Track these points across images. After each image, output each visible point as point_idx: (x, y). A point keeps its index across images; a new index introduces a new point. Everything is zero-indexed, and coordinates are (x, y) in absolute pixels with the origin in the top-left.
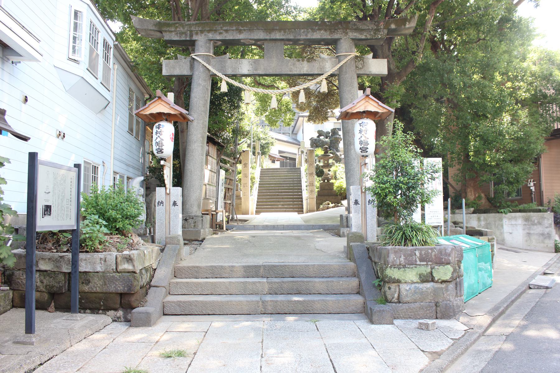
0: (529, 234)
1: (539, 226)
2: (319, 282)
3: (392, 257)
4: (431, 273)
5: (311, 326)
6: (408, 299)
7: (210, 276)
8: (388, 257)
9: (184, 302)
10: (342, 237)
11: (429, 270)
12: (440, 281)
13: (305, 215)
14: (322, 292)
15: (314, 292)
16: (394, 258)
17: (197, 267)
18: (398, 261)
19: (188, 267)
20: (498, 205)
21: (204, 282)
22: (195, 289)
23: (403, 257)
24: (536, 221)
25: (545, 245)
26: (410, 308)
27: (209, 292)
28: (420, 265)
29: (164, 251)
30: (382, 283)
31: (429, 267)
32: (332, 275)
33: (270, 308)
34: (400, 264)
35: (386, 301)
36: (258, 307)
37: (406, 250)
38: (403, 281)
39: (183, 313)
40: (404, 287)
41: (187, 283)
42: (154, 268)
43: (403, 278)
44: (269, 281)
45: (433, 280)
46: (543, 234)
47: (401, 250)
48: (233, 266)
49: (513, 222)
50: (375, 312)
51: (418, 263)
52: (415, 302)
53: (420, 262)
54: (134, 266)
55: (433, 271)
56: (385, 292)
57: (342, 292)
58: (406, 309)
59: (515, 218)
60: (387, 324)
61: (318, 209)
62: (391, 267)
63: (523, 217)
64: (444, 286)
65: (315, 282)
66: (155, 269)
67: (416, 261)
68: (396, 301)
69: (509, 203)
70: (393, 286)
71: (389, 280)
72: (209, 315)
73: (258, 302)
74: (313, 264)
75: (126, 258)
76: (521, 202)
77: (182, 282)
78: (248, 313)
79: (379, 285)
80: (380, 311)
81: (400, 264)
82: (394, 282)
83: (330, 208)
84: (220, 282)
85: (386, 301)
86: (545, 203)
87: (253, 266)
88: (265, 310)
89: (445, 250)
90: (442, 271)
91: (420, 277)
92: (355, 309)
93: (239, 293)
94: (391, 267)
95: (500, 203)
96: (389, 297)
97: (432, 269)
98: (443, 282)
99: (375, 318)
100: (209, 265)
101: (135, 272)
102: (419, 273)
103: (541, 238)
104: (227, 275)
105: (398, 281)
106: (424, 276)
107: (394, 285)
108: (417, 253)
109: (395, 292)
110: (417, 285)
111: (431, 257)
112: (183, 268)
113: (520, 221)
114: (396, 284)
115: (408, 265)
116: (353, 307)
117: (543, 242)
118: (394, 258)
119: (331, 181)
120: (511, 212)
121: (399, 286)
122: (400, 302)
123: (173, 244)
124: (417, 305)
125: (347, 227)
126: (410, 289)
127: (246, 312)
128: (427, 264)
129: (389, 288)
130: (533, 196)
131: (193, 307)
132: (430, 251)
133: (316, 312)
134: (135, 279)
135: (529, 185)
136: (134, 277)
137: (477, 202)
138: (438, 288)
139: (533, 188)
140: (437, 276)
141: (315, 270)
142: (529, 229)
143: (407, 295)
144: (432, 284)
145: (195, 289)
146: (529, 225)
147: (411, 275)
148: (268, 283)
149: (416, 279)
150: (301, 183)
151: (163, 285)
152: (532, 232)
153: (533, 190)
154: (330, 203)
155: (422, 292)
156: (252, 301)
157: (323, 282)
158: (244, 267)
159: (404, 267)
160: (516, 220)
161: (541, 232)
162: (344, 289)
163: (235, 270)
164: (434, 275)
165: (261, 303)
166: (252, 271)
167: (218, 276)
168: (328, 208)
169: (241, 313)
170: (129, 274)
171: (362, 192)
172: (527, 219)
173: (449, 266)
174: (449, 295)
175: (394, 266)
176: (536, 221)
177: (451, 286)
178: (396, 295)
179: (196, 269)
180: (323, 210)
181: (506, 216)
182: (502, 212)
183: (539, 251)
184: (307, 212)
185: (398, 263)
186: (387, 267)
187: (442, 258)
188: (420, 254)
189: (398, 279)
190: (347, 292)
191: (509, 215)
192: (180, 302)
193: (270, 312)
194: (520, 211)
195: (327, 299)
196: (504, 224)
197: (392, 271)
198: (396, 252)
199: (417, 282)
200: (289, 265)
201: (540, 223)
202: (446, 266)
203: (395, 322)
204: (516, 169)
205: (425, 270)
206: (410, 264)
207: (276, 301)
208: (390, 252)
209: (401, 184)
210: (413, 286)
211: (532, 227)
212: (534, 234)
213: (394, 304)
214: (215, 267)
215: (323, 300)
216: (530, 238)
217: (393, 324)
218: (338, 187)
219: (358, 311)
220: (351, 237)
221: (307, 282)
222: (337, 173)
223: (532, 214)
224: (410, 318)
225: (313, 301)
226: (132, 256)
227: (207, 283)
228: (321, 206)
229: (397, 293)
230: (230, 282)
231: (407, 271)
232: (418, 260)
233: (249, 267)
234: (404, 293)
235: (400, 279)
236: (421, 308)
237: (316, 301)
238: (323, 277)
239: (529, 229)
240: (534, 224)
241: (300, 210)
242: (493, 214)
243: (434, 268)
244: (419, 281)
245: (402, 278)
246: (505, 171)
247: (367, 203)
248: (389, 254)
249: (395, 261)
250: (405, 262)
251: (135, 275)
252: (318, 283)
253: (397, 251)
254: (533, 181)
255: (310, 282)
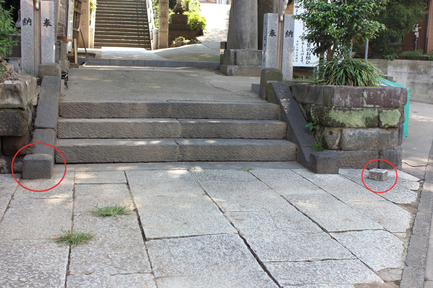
0: (413, 83)
1: (424, 75)
2: (242, 124)
3: (337, 97)
4: (378, 117)
5: (243, 174)
6: (351, 146)
7: (106, 115)
8: (333, 96)
9: (83, 147)
10: (229, 75)
11: (376, 114)
12: (387, 126)
13: (153, 51)
14: (244, 136)
15: (235, 136)
16: (339, 99)
17: (89, 104)
18: (343, 102)
19: (77, 104)
20: (381, 50)
21: (102, 123)
22: (92, 131)
23: (349, 98)
24: (422, 70)
25: (428, 96)
26: (352, 156)
27: (109, 135)
28: (366, 108)
29: (42, 84)
30: (318, 127)
31: (377, 110)
32: (251, 117)
33: (189, 154)
34: (345, 106)
35: (325, 146)
36: (175, 153)
37: (353, 90)
38: (347, 126)
39: (81, 161)
40: (348, 132)
41: (81, 123)
42: (35, 104)
43: (348, 122)
44: (184, 122)
45: (379, 126)
46: (427, 85)
47: (347, 90)
48: (134, 104)
49: (398, 70)
50: (320, 160)
51: (365, 105)
52: (358, 149)
53: (367, 104)
54: (21, 100)
55: (381, 115)
56: (324, 138)
57: (268, 136)
58: (348, 157)
59: (401, 65)
60: (332, 173)
61: (170, 45)
62: (335, 109)
63: (409, 64)
64: (389, 132)
65: (237, 124)
66: (36, 107)
67: (363, 103)
68: (336, 147)
69: (392, 49)
70: (335, 131)
71: (332, 123)
72: (114, 163)
73: (175, 147)
74: (230, 103)
75: (10, 90)
76: (405, 48)
77: (74, 123)
78: (163, 160)
79: (314, 130)
80: (325, 159)
81: (345, 106)
82: (337, 127)
83: (185, 44)
84: (123, 123)
85: (325, 146)
86: (428, 51)
87: (159, 104)
88: (183, 157)
89: (395, 93)
90: (390, 116)
91: (366, 121)
92: (286, 157)
93: (147, 136)
94: (335, 109)
95: (383, 48)
96: (330, 143)
97: (379, 112)
98: (391, 127)
99: (319, 166)
100: (104, 101)
101: (22, 109)
102: (365, 117)
103: (426, 88)
104: (127, 115)
105: (342, 126)
106: (371, 121)
107: (336, 129)
108: (365, 94)
109: (337, 137)
110: (362, 130)
111: (380, 99)
112: (71, 105)
113: (405, 69)
114: (339, 129)
115: (354, 107)
116: (284, 154)
117: (427, 93)
118: (339, 99)
119: (185, 13)
120: (397, 59)
121: (341, 131)
122: (341, 149)
123: (49, 75)
124: (360, 152)
125: (235, 64)
126: (353, 134)
127: (160, 159)
128: (374, 107)
129: (331, 133)
130: (416, 42)
131: (95, 154)
132: (379, 92)
133: (242, 159)
134: (24, 117)
135: (414, 31)
136: (22, 115)
137: (359, 45)
138: (384, 134)
139: (417, 34)
140: (384, 121)
141: (233, 110)
142: (414, 78)
143: (350, 142)
144: (378, 129)
145: (92, 131)
146: (414, 74)
147: (357, 119)
148: (181, 124)
149: (361, 123)
150: (146, 14)
151: (51, 126)
152: (416, 81)
153: (418, 36)
154: (184, 39)
155: (367, 138)
156: (169, 146)
157: (246, 125)
158: (148, 105)
159: (350, 109)
160: (401, 68)
161: (425, 82)
162: (268, 133)
163: (137, 108)
164: (381, 120)
165: (178, 148)
166: (157, 110)
167: (116, 115)
168: (183, 44)
169: (154, 160)
170: (15, 111)
171: (280, 21)
172: (413, 67)
173: (397, 110)
174: (393, 143)
175: (339, 108)
176: (422, 70)
177: (396, 132)
178: (337, 141)
179: (88, 107)
180: (176, 46)
181: (392, 62)
182: (387, 58)
183: (421, 102)
184: (157, 48)
185: (343, 105)
186: (330, 109)
187: (391, 101)
188: (369, 95)
189: (342, 123)
190: (272, 136)
191: (395, 61)
192: (78, 147)
193: (189, 159)
194: (406, 58)
195: (254, 144)
196: (389, 71)
197: (336, 114)
198: (341, 92)
199: (362, 128)
200: (202, 104)
201: (426, 72)
202: (394, 111)
203: (341, 171)
204: (410, 12)
205: (372, 113)
206: (356, 105)
207: (197, 146)
208: (336, 91)
209: (344, 13)
210: (357, 131)
211: (418, 76)
212: (418, 83)
213: (335, 151)
214: (112, 104)
215: (251, 145)
216: (414, 88)
217: (337, 173)
218: (191, 21)
219: (289, 159)
220: (268, 73)
221: (228, 124)
222: (190, 4)
223: (419, 62)
224: (352, 167)
225: (240, 147)
226: (18, 87)
227: (106, 123)
228: (174, 42)
229: (339, 138)
230: (136, 123)
231: (353, 114)
232: (365, 102)
233: (154, 105)
234: (347, 138)
235: (345, 123)
236: (364, 156)
237: (243, 146)
238: (242, 119)
239: (414, 78)
240: (419, 73)
241: (148, 47)
242: (378, 60)
243: (381, 112)
244: (364, 126)
245: (346, 122)
246: (397, 13)
247: (285, 35)
248: (334, 93)
249: (340, 102)
250: (351, 104)
251: (23, 112)
252: (241, 126)
253: (343, 91)
254: (418, 26)
255: (231, 124)
